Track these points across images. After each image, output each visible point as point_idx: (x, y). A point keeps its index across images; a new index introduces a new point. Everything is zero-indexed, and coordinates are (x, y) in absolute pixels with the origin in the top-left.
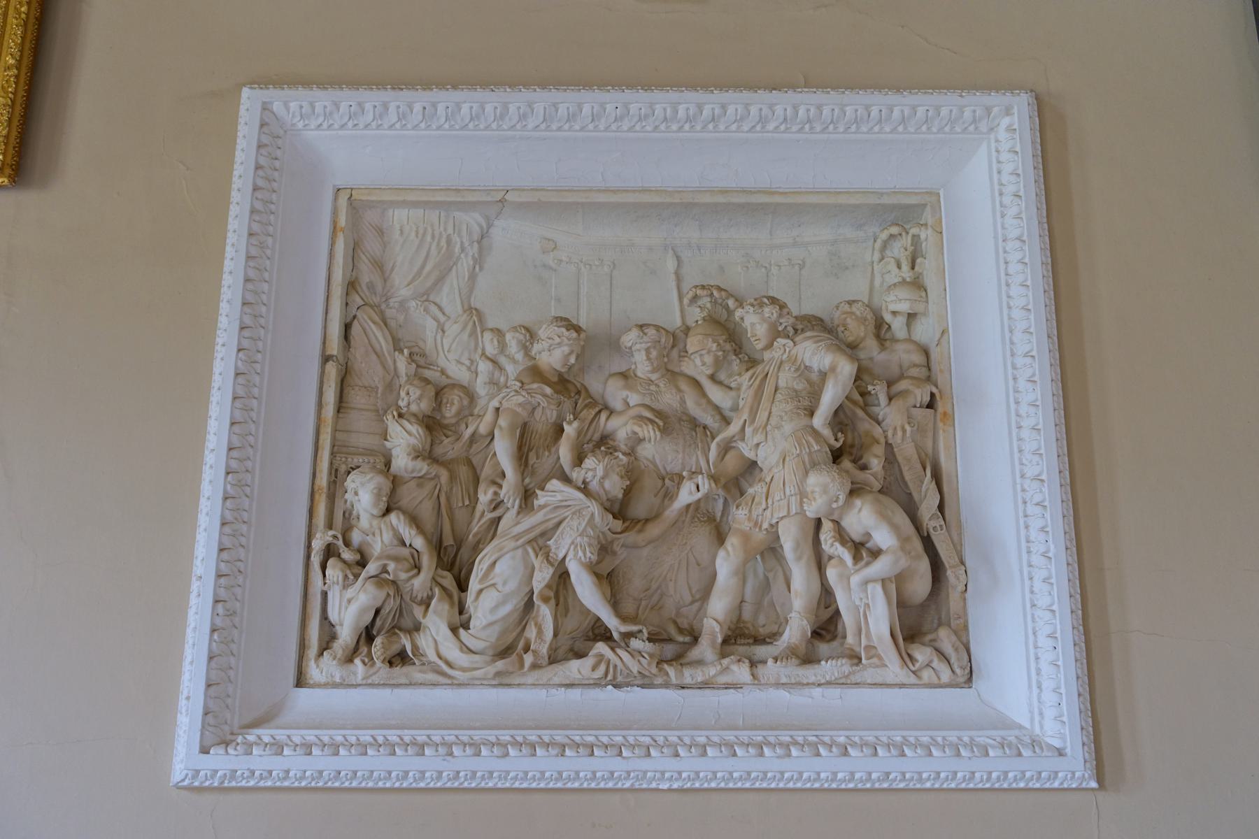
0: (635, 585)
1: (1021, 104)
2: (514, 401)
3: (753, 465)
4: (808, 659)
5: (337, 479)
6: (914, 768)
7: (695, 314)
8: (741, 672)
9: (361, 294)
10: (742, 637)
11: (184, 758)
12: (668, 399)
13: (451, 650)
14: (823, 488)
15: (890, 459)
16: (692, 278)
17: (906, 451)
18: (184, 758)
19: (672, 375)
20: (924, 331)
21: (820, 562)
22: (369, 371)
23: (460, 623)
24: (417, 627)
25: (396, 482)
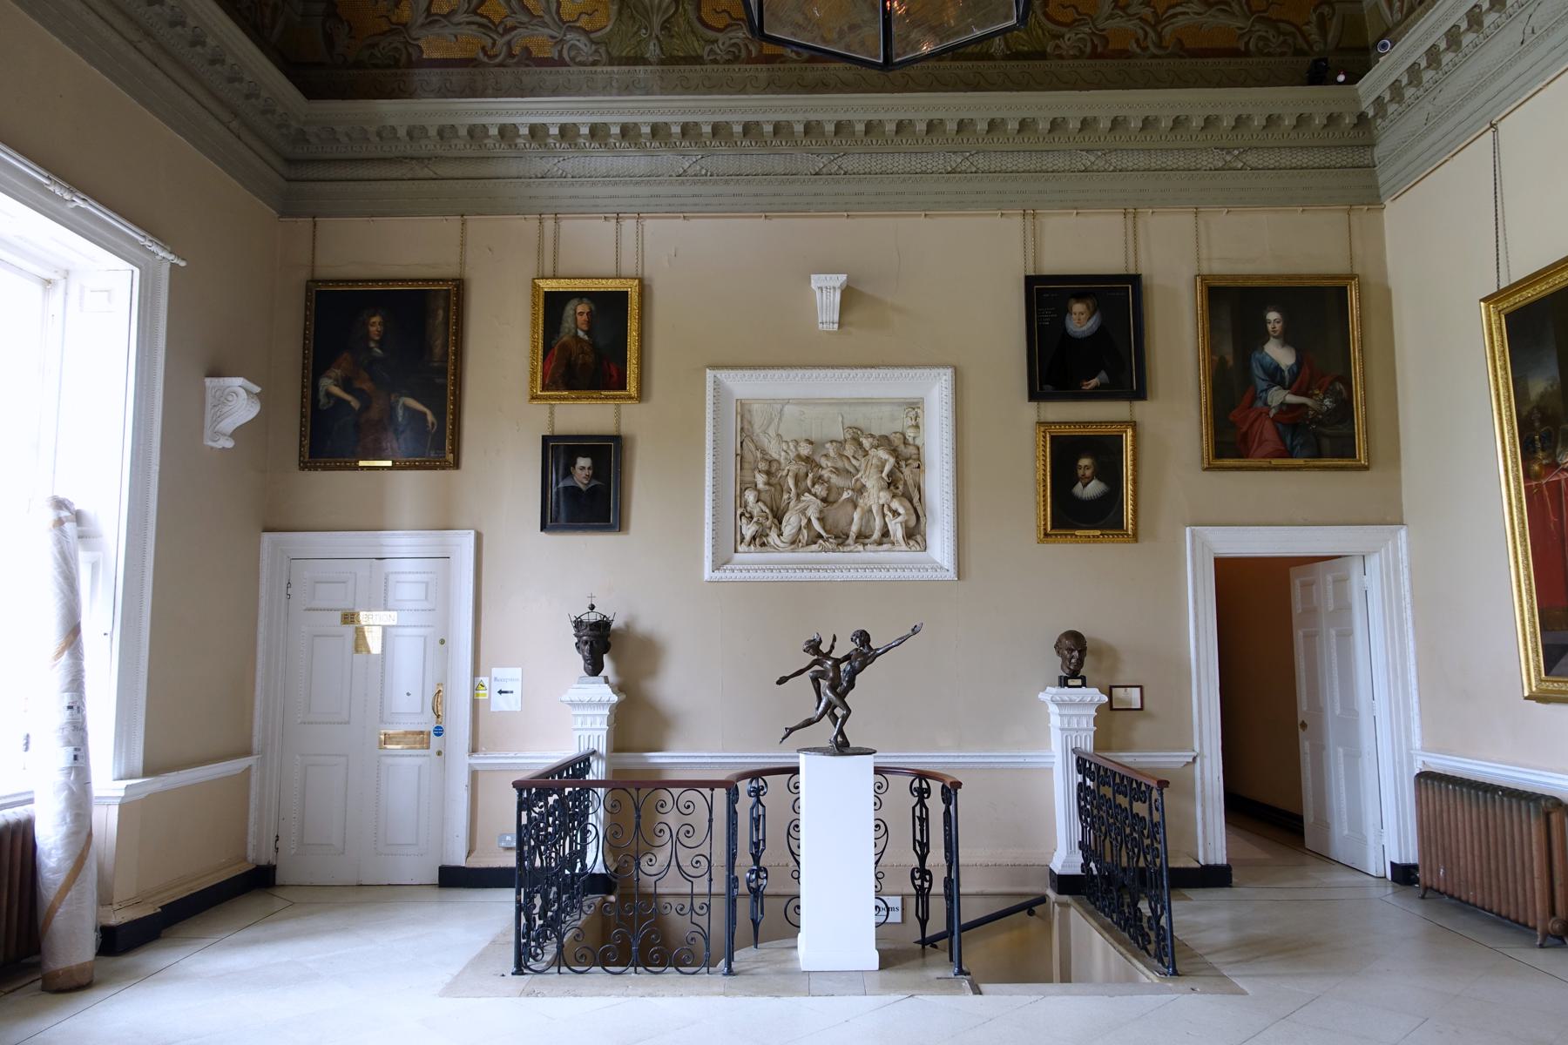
0: (830, 521)
1: (949, 372)
2: (794, 467)
3: (864, 486)
4: (880, 544)
5: (743, 491)
6: (907, 575)
7: (848, 436)
8: (860, 548)
9: (745, 433)
10: (862, 537)
11: (708, 573)
12: (840, 464)
13: (778, 542)
14: (884, 496)
15: (905, 484)
16: (847, 424)
17: (910, 482)
18: (708, 573)
19: (841, 455)
20: (918, 442)
21: (884, 516)
22: (749, 457)
23: (780, 535)
24: (393, 128)
25: (759, 492)
